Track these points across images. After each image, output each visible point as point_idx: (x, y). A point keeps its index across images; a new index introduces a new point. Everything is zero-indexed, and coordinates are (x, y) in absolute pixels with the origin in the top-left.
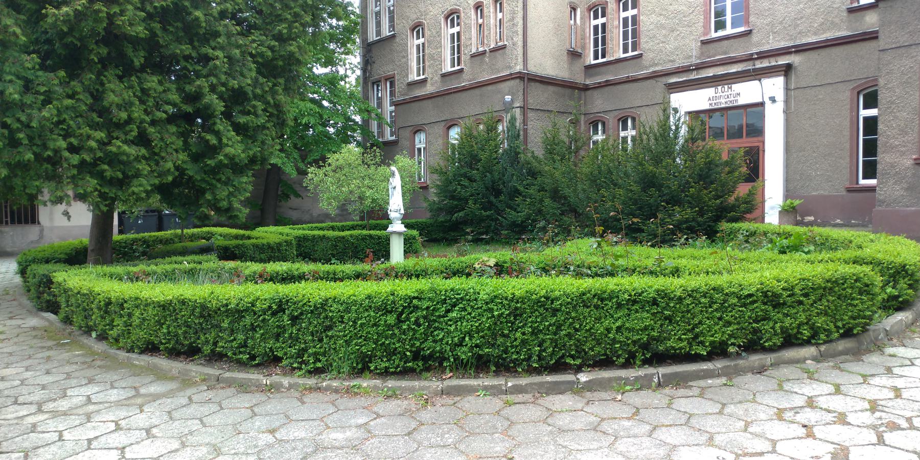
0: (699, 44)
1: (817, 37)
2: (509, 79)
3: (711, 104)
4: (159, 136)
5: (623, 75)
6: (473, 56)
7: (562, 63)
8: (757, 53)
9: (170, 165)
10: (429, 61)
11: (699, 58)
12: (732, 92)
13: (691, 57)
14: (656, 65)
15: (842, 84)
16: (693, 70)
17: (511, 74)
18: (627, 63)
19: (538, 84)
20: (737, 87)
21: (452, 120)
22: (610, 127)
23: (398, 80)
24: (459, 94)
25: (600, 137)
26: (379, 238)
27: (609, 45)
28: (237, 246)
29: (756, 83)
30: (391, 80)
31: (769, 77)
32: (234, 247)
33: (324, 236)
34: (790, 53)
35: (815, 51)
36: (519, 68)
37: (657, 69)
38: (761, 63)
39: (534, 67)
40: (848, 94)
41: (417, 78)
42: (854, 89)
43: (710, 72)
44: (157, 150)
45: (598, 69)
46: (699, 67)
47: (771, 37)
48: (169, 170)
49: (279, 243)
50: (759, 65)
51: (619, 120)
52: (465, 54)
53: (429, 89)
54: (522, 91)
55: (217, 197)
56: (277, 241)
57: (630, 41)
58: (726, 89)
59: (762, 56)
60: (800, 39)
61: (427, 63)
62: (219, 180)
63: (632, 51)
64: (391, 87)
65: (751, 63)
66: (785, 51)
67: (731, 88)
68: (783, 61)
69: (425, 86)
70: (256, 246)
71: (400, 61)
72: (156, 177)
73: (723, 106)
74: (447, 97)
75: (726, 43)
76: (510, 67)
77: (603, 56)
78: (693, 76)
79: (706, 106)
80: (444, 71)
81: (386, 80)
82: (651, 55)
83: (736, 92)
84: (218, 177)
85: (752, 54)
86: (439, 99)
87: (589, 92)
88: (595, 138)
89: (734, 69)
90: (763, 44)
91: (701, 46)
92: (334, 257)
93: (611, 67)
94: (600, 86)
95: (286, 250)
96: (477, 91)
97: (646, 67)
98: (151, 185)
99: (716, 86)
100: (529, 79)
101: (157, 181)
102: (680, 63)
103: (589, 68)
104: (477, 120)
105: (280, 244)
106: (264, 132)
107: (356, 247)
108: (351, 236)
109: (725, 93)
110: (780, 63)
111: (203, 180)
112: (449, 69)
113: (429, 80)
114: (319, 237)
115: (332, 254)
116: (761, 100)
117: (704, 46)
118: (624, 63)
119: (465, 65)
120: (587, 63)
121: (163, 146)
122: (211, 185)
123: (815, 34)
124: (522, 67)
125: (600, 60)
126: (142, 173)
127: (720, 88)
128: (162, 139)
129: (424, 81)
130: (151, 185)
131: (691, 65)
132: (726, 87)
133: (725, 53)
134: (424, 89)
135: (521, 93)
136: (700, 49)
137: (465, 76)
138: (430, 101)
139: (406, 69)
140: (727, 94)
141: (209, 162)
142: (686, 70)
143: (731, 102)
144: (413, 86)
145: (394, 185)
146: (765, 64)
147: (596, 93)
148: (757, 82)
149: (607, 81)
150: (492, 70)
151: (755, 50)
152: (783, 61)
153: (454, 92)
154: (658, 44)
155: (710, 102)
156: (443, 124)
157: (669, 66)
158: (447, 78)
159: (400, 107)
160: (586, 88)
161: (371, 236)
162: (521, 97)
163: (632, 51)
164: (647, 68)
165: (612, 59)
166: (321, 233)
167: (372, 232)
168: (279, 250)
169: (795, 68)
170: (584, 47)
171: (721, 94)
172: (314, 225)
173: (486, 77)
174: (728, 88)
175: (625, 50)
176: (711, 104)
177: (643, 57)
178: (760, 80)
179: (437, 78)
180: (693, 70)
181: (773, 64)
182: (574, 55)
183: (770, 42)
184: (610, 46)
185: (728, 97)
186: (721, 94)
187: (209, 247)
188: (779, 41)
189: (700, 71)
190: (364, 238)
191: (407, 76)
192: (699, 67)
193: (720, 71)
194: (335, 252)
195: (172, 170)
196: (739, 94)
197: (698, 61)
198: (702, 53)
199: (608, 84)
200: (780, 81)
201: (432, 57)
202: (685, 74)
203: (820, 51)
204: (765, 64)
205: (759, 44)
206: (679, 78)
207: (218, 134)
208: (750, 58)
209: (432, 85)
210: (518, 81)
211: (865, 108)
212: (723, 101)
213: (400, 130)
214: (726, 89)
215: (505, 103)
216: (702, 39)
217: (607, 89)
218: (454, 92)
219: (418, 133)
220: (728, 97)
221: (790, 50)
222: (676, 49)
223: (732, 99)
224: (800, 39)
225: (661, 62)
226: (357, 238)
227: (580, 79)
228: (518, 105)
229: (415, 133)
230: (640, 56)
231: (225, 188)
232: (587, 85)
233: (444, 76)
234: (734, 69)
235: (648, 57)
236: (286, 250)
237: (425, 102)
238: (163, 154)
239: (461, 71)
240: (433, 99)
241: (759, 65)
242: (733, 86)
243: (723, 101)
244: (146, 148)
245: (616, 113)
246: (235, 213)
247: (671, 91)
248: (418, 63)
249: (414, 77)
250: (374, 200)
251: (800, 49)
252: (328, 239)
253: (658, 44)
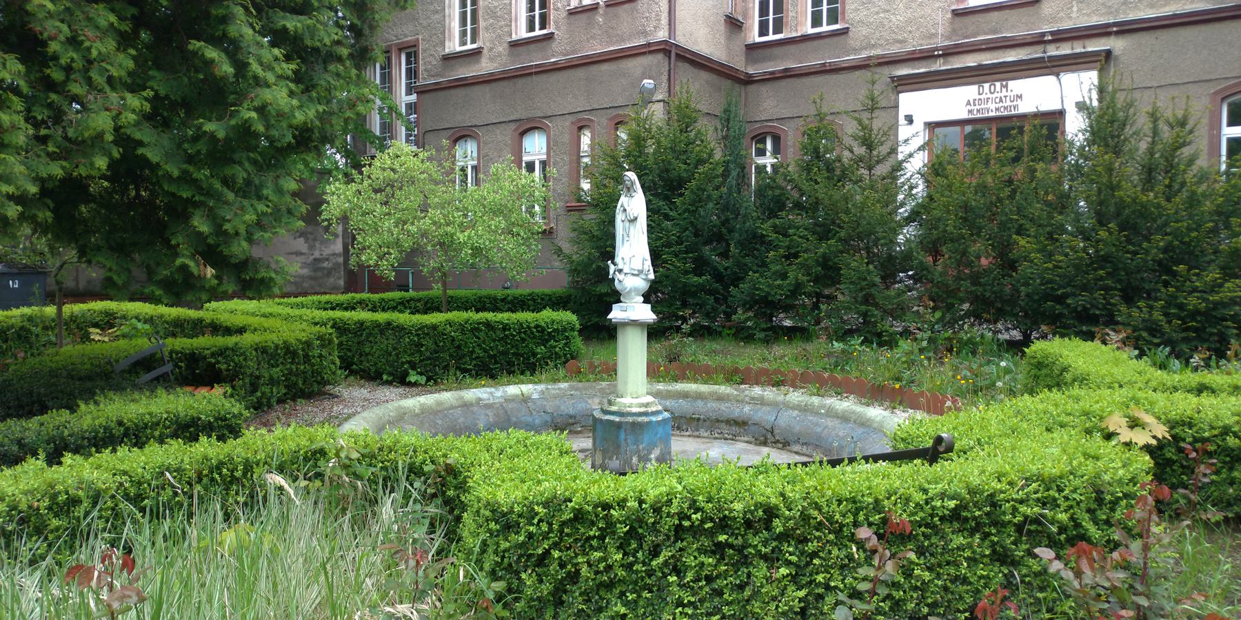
0: (949, 15)
1: (1154, 11)
2: (644, 53)
3: (970, 112)
4: (65, 28)
5: (815, 62)
6: (572, 13)
7: (717, 36)
8: (1052, 33)
9: (102, 122)
10: (485, 20)
11: (949, 38)
12: (1009, 93)
13: (934, 35)
14: (874, 46)
15: (1196, 86)
16: (939, 56)
17: (649, 45)
18: (822, 42)
19: (687, 65)
20: (1016, 86)
21: (529, 120)
22: (790, 143)
23: (424, 51)
24: (544, 76)
25: (768, 161)
26: (506, 327)
27: (790, 13)
28: (222, 352)
29: (1051, 79)
30: (411, 50)
31: (1073, 71)
32: (213, 355)
33: (389, 324)
34: (1108, 34)
35: (1152, 31)
36: (662, 35)
37: (873, 53)
38: (1057, 48)
39: (681, 40)
40: (1206, 101)
41: (459, 49)
42: (1216, 93)
43: (971, 61)
44: (57, 76)
45: (768, 52)
46: (948, 53)
47: (1075, 9)
48: (100, 136)
49: (306, 342)
50: (1053, 51)
51: (753, 138)
52: (557, 9)
53: (485, 66)
54: (666, 74)
55: (227, 226)
56: (303, 336)
57: (771, 17)
58: (998, 88)
59: (1060, 37)
60: (1124, 12)
61: (482, 24)
62: (227, 182)
63: (774, 34)
64: (408, 62)
65: (1040, 48)
66: (1102, 31)
67: (1006, 86)
68: (1094, 46)
69: (478, 62)
70: (262, 350)
71: (429, 18)
72: (52, 157)
73: (992, 114)
74: (521, 82)
75: (996, 14)
76: (645, 33)
77: (778, 29)
78: (939, 65)
79: (963, 114)
80: (514, 37)
81: (400, 50)
82: (864, 31)
83: (1015, 93)
84: (228, 171)
85: (1043, 34)
86: (505, 83)
87: (753, 87)
88: (761, 161)
89: (1011, 56)
90: (1061, 19)
91: (953, 18)
92: (414, 368)
93: (792, 48)
94: (773, 78)
95: (321, 356)
96: (580, 73)
97: (855, 50)
98: (38, 179)
99: (980, 83)
100: (678, 55)
101: (56, 170)
102: (915, 44)
103: (752, 48)
104: (580, 120)
105: (308, 344)
106: (332, 67)
107: (459, 347)
108: (450, 323)
109: (996, 95)
110: (1090, 49)
111: (186, 178)
112: (522, 33)
113: (485, 51)
114: (377, 325)
115: (409, 362)
116: (1060, 108)
117: (958, 19)
118: (815, 43)
119: (557, 28)
120: (750, 41)
121: (79, 64)
122: (209, 193)
123: (1152, 6)
124: (667, 34)
125: (771, 37)
126: (7, 138)
127: (986, 86)
128: (73, 42)
129: (477, 53)
130: (38, 179)
131: (937, 49)
132: (998, 84)
133: (994, 32)
134: (476, 67)
135: (665, 78)
136: (951, 23)
137: (555, 46)
138: (486, 88)
139: (441, 33)
140: (999, 95)
141: (209, 127)
142: (926, 56)
143: (978, 111)
144: (453, 62)
145: (632, 214)
146: (1065, 49)
147: (764, 89)
148: (1052, 78)
149: (786, 70)
150: (609, 37)
151: (1046, 28)
152: (1094, 46)
153: (536, 73)
154: (877, 13)
155: (969, 107)
156: (513, 126)
157: (895, 49)
158: (521, 49)
159: (426, 96)
160: (748, 81)
161: (488, 324)
162: (665, 85)
163: (774, 34)
164: (855, 51)
165: (794, 35)
166: (381, 317)
167: (490, 316)
168: (306, 356)
169: (1117, 58)
170: (745, 15)
171: (989, 95)
172: (331, 298)
173: (597, 48)
174: (1002, 86)
175: (816, 22)
176: (970, 112)
177: (850, 34)
178: (1057, 75)
179: (502, 48)
180: (939, 56)
181: (1079, 50)
182: (734, 24)
183: (1074, 15)
184: (791, 14)
185: (1001, 101)
186: (989, 95)
187: (153, 355)
188: (1088, 15)
189: (951, 59)
190: (475, 329)
191: (443, 43)
192: (948, 53)
193: (988, 59)
194: (417, 358)
195: (109, 137)
196: (1020, 97)
197: (947, 43)
198: (954, 31)
199: (788, 74)
200: (1090, 77)
201: (492, 13)
202: (924, 63)
203: (1159, 33)
204: (1065, 49)
205: (1053, 19)
206: (913, 69)
207: (233, 49)
208: (1039, 40)
209: (491, 59)
210: (660, 56)
211: (1230, 124)
212: (992, 106)
213: (428, 136)
214: (998, 88)
215: (643, 91)
216: (954, 7)
217: (784, 83)
218: (536, 73)
219: (462, 142)
220: (1001, 101)
221: (1109, 30)
222: (909, 22)
223: (1009, 103)
224: (1124, 12)
225: (882, 42)
226: (462, 327)
227: (739, 63)
228: (660, 97)
229: (456, 141)
230: (845, 32)
231: (246, 203)
232: (751, 76)
233: (515, 45)
234: (1011, 56)
235: (859, 33)
236: (321, 356)
237: (476, 88)
238: (76, 89)
239: (550, 37)
240: (494, 85)
241: (1053, 51)
242: (1011, 83)
243: (992, 106)
244: (22, 61)
245: (801, 122)
246: (263, 274)
247: (899, 88)
248: (463, 22)
249: (454, 45)
250: (477, 251)
251: (1126, 29)
252: (400, 329)
253: (877, 13)
